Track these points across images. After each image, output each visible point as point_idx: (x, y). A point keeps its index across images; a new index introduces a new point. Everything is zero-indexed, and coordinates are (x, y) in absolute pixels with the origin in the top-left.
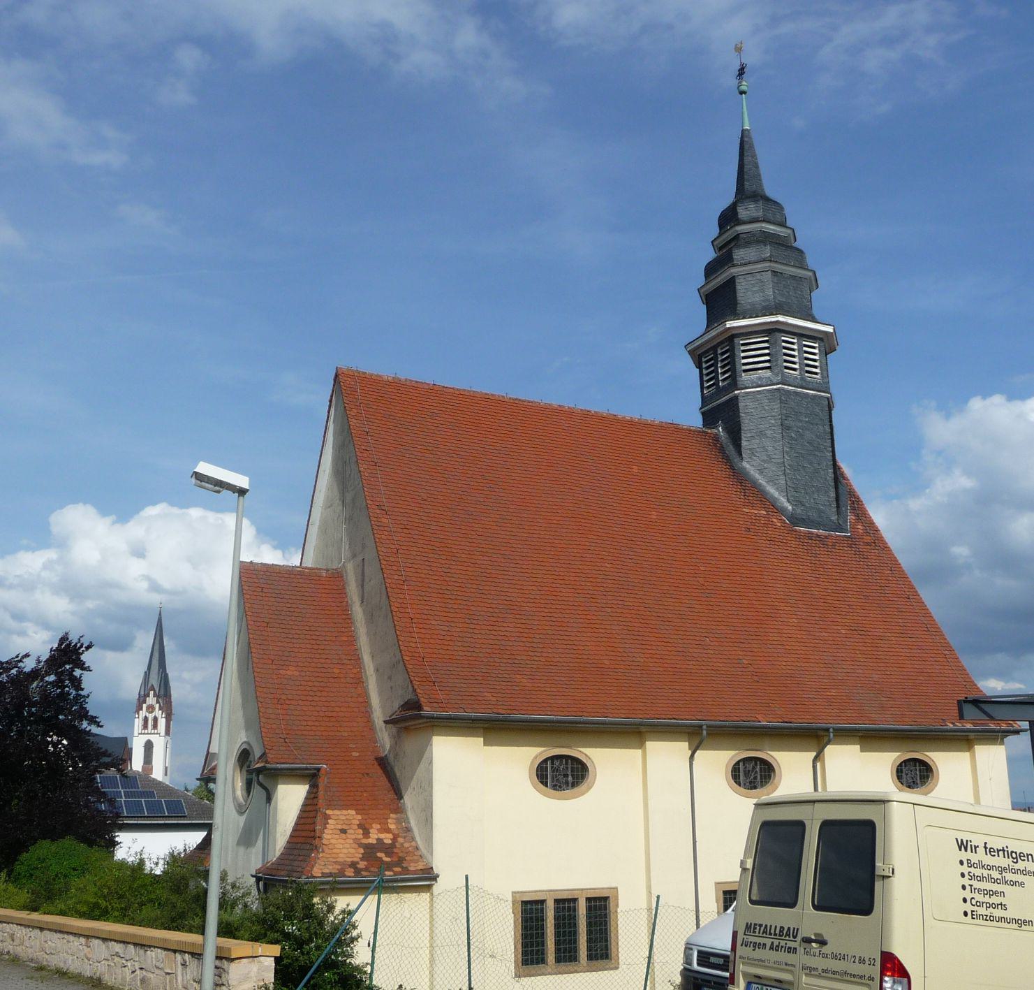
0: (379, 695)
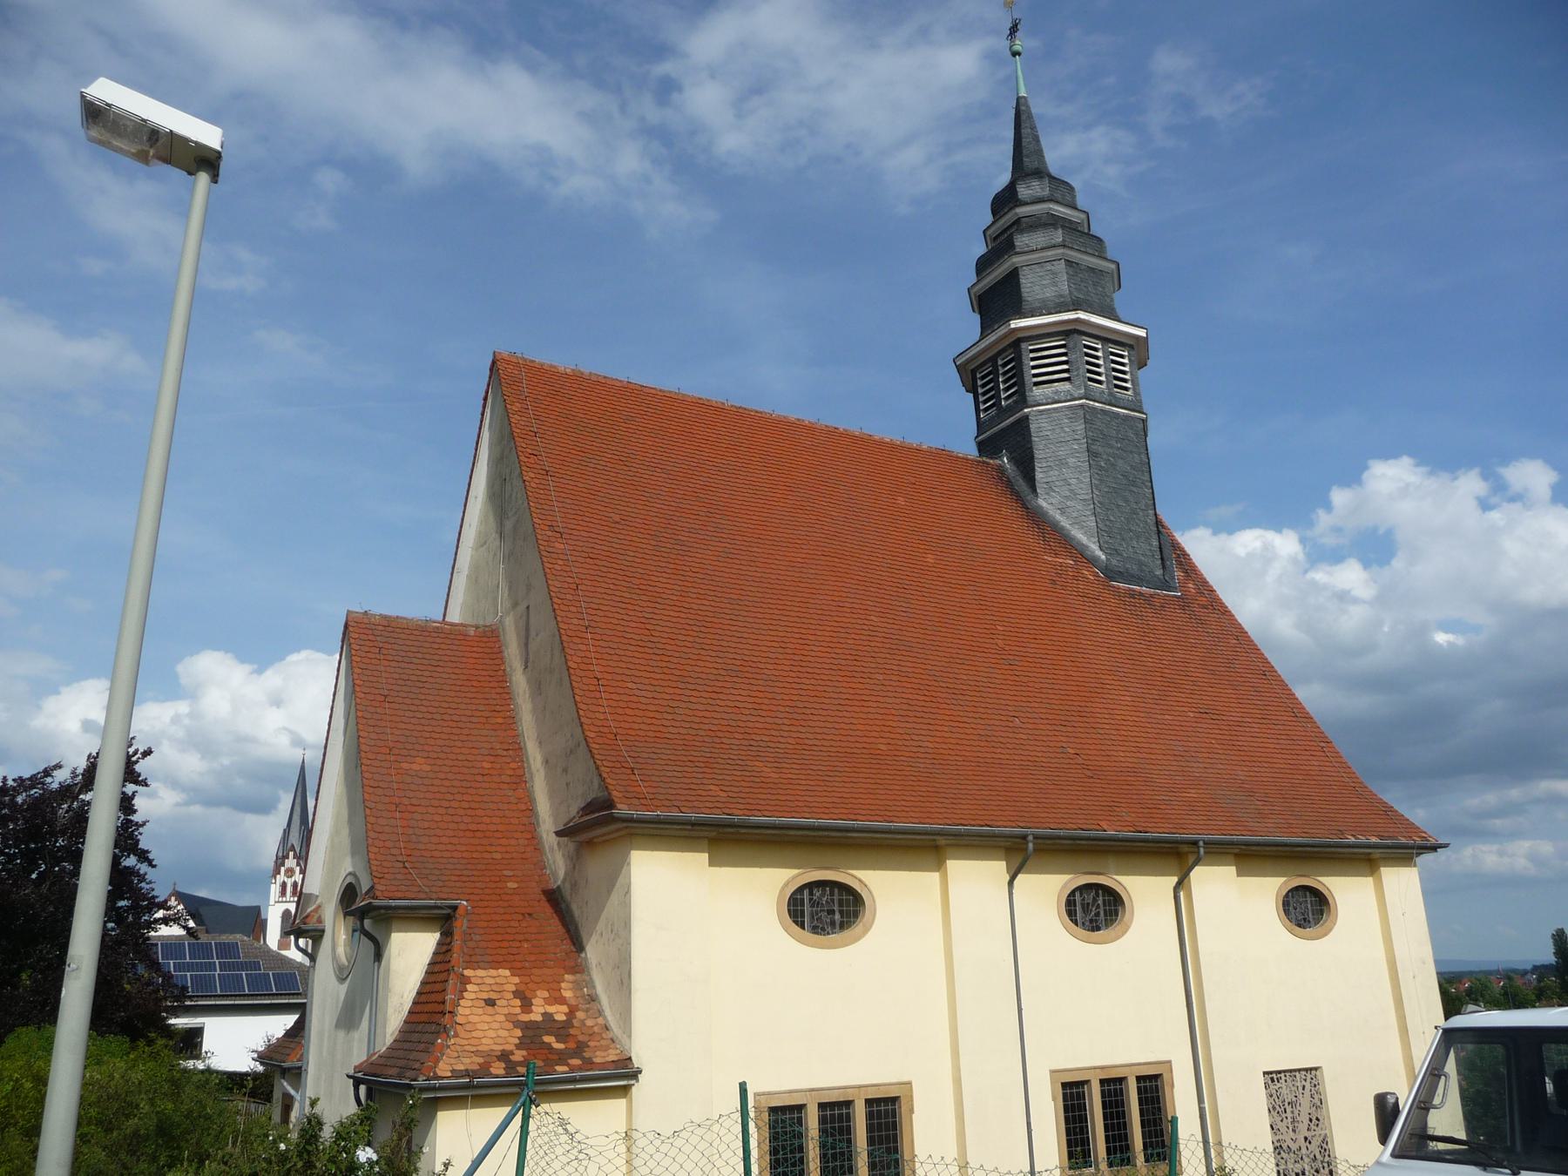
0: (549, 799)
